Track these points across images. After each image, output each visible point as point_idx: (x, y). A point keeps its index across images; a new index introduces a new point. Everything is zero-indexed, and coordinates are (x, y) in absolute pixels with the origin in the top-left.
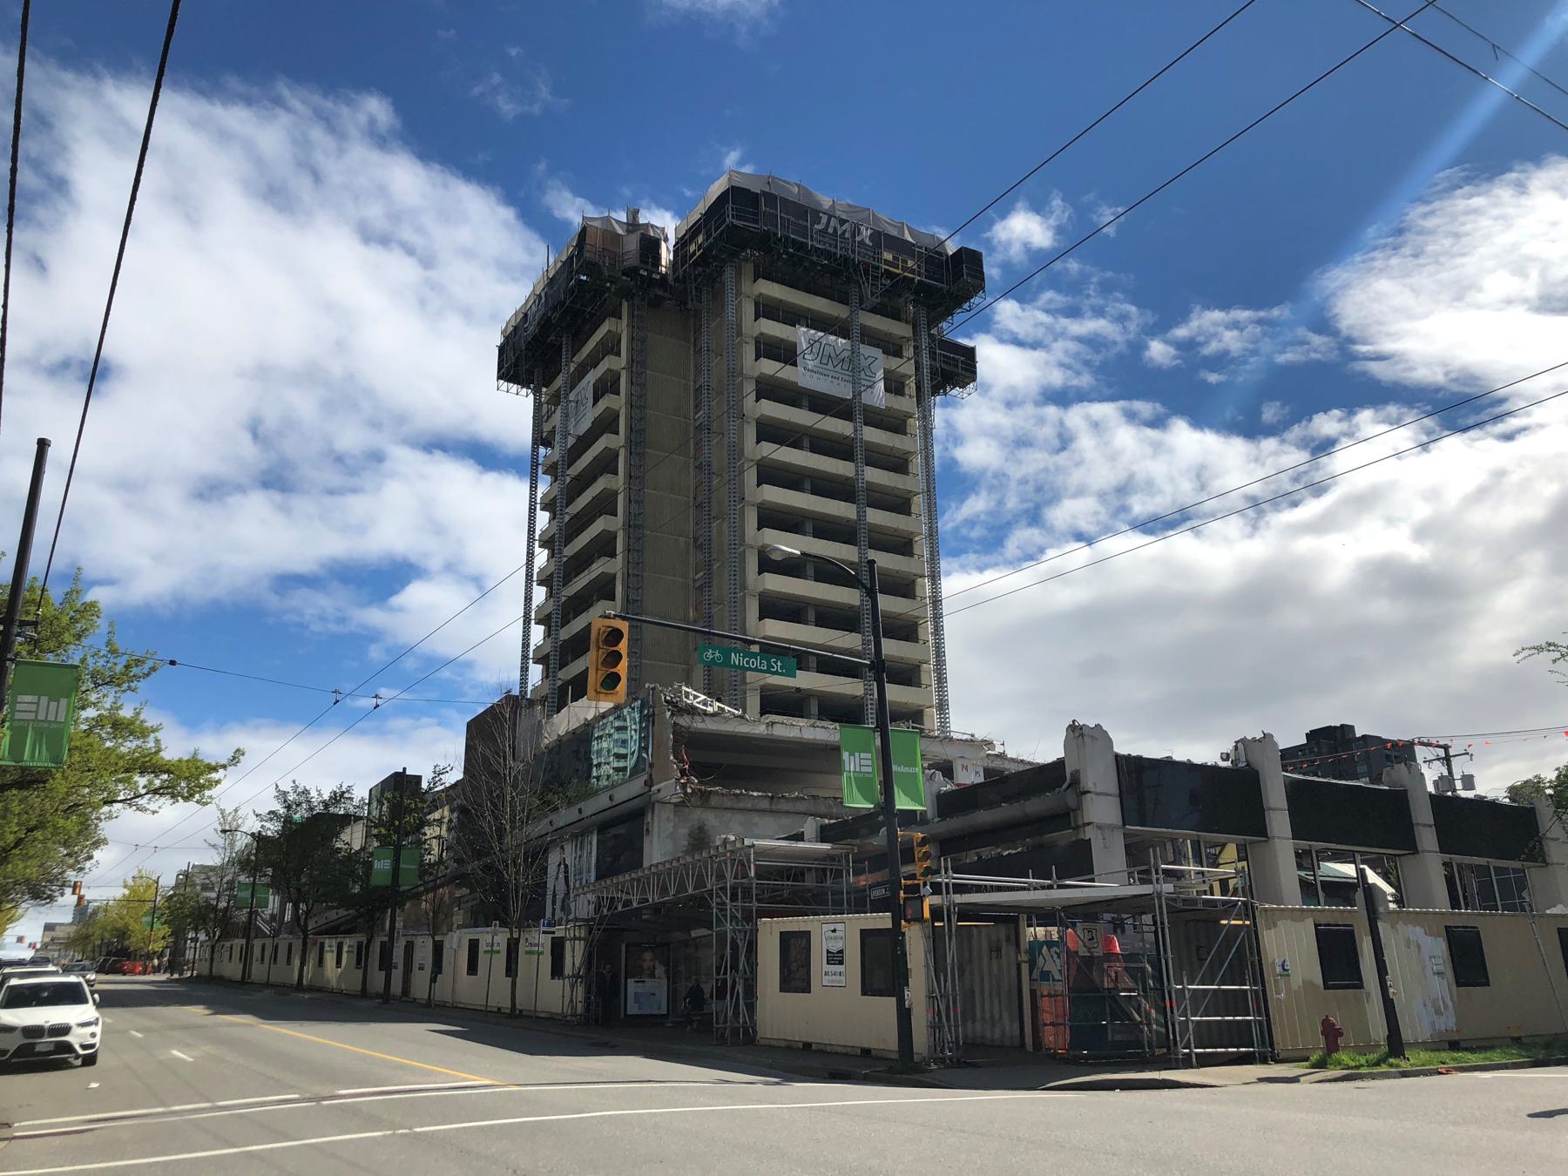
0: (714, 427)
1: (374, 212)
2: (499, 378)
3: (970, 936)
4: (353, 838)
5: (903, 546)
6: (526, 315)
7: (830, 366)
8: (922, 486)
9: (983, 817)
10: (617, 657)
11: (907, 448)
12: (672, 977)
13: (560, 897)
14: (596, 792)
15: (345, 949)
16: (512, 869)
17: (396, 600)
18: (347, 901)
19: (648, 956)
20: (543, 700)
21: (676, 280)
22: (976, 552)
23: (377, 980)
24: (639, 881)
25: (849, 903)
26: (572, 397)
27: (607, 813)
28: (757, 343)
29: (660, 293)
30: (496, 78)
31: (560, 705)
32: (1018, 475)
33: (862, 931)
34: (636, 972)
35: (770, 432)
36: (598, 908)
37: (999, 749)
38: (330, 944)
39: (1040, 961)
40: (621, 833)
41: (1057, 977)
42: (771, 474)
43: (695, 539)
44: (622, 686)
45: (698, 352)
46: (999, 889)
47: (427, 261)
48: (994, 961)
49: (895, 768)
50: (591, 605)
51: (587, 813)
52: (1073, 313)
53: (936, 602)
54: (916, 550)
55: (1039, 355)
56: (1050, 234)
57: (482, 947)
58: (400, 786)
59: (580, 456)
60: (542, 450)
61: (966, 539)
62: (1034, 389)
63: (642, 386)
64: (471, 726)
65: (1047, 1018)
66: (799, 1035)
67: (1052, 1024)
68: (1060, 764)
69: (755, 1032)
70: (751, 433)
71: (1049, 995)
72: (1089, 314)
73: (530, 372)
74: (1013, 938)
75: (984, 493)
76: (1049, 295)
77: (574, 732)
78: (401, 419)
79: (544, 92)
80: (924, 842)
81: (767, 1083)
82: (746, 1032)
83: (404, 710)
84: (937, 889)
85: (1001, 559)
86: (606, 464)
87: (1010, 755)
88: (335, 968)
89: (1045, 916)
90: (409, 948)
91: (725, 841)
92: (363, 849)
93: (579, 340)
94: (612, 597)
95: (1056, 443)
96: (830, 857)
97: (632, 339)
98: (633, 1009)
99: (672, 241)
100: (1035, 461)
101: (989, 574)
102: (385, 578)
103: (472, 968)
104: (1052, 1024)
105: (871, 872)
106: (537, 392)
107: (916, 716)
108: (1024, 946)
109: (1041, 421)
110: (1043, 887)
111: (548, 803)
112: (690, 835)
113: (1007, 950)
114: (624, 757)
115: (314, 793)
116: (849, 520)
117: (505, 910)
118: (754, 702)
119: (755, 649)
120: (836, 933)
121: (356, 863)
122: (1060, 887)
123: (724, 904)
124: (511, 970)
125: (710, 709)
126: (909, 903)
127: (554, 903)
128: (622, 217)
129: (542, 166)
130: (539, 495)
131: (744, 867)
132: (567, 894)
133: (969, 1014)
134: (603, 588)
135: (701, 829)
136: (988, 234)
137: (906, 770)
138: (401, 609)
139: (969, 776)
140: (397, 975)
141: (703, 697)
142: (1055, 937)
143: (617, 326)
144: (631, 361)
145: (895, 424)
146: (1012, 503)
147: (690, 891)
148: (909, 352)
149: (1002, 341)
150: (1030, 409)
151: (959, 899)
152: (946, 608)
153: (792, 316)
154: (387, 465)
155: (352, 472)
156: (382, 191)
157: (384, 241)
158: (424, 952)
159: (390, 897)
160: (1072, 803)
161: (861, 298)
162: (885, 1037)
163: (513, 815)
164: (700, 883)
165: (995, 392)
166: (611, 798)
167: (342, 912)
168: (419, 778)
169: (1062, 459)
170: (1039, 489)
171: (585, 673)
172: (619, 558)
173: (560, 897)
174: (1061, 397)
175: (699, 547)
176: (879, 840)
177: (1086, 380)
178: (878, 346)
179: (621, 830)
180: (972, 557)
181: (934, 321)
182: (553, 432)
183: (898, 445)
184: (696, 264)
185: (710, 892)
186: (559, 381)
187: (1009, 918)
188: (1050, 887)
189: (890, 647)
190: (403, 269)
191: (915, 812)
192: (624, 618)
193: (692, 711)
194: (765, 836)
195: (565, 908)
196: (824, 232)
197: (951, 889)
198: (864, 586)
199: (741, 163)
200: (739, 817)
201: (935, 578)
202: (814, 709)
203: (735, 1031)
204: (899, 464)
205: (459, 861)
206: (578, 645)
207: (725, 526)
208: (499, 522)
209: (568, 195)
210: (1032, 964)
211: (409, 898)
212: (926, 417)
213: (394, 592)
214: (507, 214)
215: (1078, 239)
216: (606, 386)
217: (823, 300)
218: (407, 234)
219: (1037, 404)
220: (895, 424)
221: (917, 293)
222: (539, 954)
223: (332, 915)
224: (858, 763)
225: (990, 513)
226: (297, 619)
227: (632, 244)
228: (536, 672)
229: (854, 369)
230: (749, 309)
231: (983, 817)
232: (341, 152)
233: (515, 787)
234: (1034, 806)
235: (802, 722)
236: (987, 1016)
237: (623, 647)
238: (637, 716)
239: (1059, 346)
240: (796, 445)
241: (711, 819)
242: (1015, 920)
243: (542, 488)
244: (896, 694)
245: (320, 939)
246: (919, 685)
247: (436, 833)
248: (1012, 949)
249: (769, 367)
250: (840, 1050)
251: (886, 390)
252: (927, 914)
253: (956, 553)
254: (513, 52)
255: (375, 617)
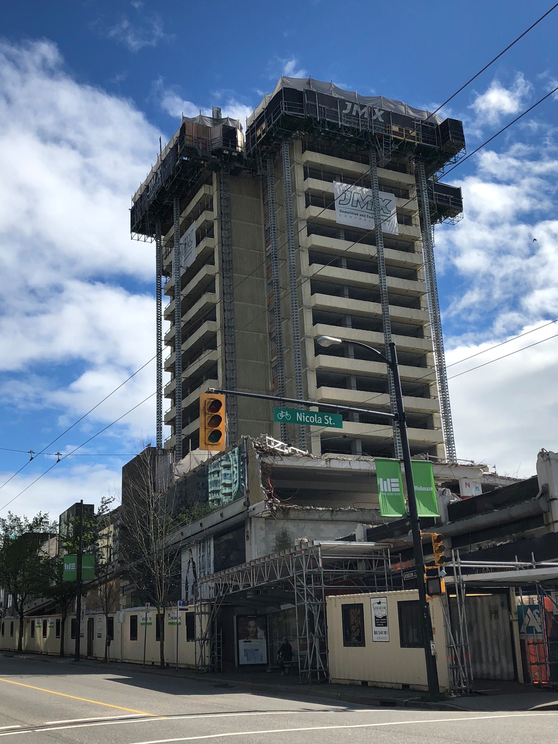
0: (279, 256)
1: (48, 122)
2: (132, 231)
3: (475, 603)
4: (50, 549)
5: (416, 331)
6: (148, 187)
7: (359, 208)
8: (427, 288)
9: (481, 520)
10: (218, 420)
11: (415, 262)
12: (269, 637)
13: (190, 584)
14: (212, 511)
15: (48, 625)
16: (157, 567)
17: (75, 385)
18: (49, 592)
19: (252, 623)
20: (173, 450)
21: (249, 156)
22: (473, 331)
23: (71, 644)
24: (243, 572)
25: (389, 583)
26: (182, 241)
27: (220, 525)
28: (307, 195)
29: (238, 165)
30: (126, 24)
31: (185, 453)
32: (501, 275)
33: (399, 603)
34: (245, 635)
35: (318, 256)
36: (217, 591)
37: (491, 471)
38: (38, 621)
39: (526, 620)
40: (230, 540)
41: (539, 630)
42: (320, 286)
43: (270, 334)
44: (224, 438)
45: (266, 204)
46: (495, 570)
47: (85, 152)
48: (494, 621)
49: (416, 488)
50: (202, 383)
51: (205, 526)
52: (535, 157)
53: (442, 369)
54: (426, 333)
55: (512, 189)
56: (516, 103)
57: (140, 621)
58: (80, 512)
59: (189, 282)
60: (163, 279)
61: (468, 323)
62: (510, 213)
63: (229, 230)
64: (126, 469)
65: (533, 659)
66: (359, 676)
67: (537, 664)
68: (534, 479)
69: (328, 674)
70: (305, 258)
71: (534, 643)
72: (547, 158)
73: (153, 226)
74: (506, 602)
75: (477, 289)
76: (518, 146)
77: (194, 471)
78: (72, 262)
79: (158, 32)
80: (439, 539)
81: (337, 711)
82: (321, 673)
83: (84, 459)
84: (450, 571)
85: (491, 335)
86: (207, 286)
87: (500, 474)
88: (42, 638)
89: (528, 587)
90: (91, 622)
91: (301, 543)
92: (57, 556)
93: (185, 201)
94: (215, 377)
95: (527, 251)
96: (376, 552)
97: (220, 198)
98: (243, 660)
99: (244, 130)
100: (512, 264)
101: (484, 346)
102: (66, 371)
103: (134, 635)
104: (537, 664)
105: (404, 560)
106: (157, 238)
107: (431, 449)
108: (514, 609)
109: (515, 236)
110: (526, 568)
111: (179, 520)
112: (277, 539)
113: (503, 612)
114: (230, 486)
115: (22, 520)
116: (377, 315)
117: (154, 595)
118: (316, 445)
119: (316, 409)
120: (381, 605)
121: (53, 565)
122: (538, 567)
123: (302, 586)
124: (160, 635)
125: (286, 451)
126: (430, 582)
127: (187, 588)
128: (209, 114)
129: (160, 82)
130: (163, 310)
131: (314, 560)
132: (195, 583)
133: (477, 658)
134: (209, 371)
135: (284, 534)
136: (472, 106)
137: (424, 489)
138: (79, 391)
139: (471, 491)
140: (84, 642)
141: (280, 443)
142: (536, 602)
143: (210, 190)
144: (221, 214)
145: (406, 245)
146: (497, 294)
147: (278, 578)
148: (413, 194)
149: (485, 181)
150: (507, 228)
151: (466, 578)
152: (449, 373)
153: (330, 175)
154: (65, 295)
155: (42, 300)
156: (53, 107)
157: (57, 140)
158: (101, 626)
159: (76, 588)
160: (544, 507)
161: (378, 159)
162: (419, 676)
163: (156, 529)
164: (285, 573)
165: (482, 217)
166: (222, 515)
167: (45, 600)
168: (92, 506)
169: (532, 262)
170: (516, 284)
171: (197, 432)
172: (219, 349)
173: (190, 584)
174: (529, 218)
175: (273, 339)
176: (408, 539)
177: (547, 205)
178: (391, 192)
179: (230, 536)
180: (471, 335)
181: (430, 172)
182: (170, 266)
183: (409, 260)
184: (262, 143)
185: (292, 579)
186: (172, 231)
187: (503, 590)
188: (531, 567)
189: (409, 402)
190: (69, 159)
191: (433, 518)
192: (222, 392)
193: (273, 453)
194: (328, 538)
195: (195, 592)
196: (349, 115)
197: (457, 571)
198: (387, 361)
199: (296, 70)
200: (310, 525)
201: (440, 352)
202: (359, 448)
203: (314, 675)
204: (411, 274)
205: (121, 562)
206: (192, 412)
207: (290, 323)
208: (137, 327)
209: (178, 100)
210: (521, 622)
211: (90, 589)
212: (428, 240)
213: (74, 380)
214: (138, 116)
215: (536, 105)
216: (205, 232)
217: (352, 163)
218: (71, 135)
219: (512, 224)
220: (406, 245)
221: (417, 153)
222: (178, 624)
223: (39, 602)
224: (389, 485)
225: (482, 303)
226: (10, 401)
227: (217, 133)
228: (167, 430)
229: (375, 209)
230: (300, 172)
231: (481, 520)
232: (24, 82)
233: (156, 510)
234: (517, 510)
235: (350, 457)
236: (491, 659)
237: (222, 412)
238: (237, 457)
239: (526, 182)
240: (337, 264)
241: (291, 527)
242: (506, 592)
243: (166, 304)
244: (414, 434)
245: (32, 618)
246: (432, 428)
247: (106, 541)
248: (506, 611)
249: (315, 211)
250: (388, 686)
251: (400, 222)
252: (443, 589)
253: (459, 333)
254: (137, 5)
255: (61, 397)
